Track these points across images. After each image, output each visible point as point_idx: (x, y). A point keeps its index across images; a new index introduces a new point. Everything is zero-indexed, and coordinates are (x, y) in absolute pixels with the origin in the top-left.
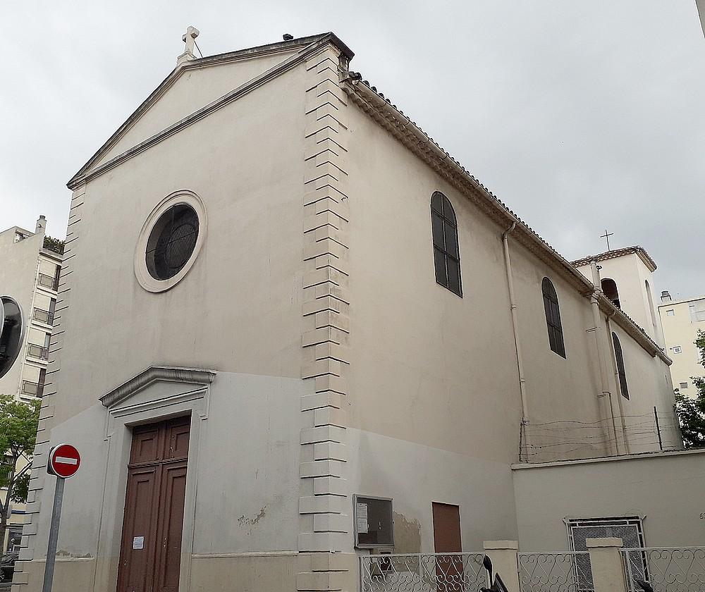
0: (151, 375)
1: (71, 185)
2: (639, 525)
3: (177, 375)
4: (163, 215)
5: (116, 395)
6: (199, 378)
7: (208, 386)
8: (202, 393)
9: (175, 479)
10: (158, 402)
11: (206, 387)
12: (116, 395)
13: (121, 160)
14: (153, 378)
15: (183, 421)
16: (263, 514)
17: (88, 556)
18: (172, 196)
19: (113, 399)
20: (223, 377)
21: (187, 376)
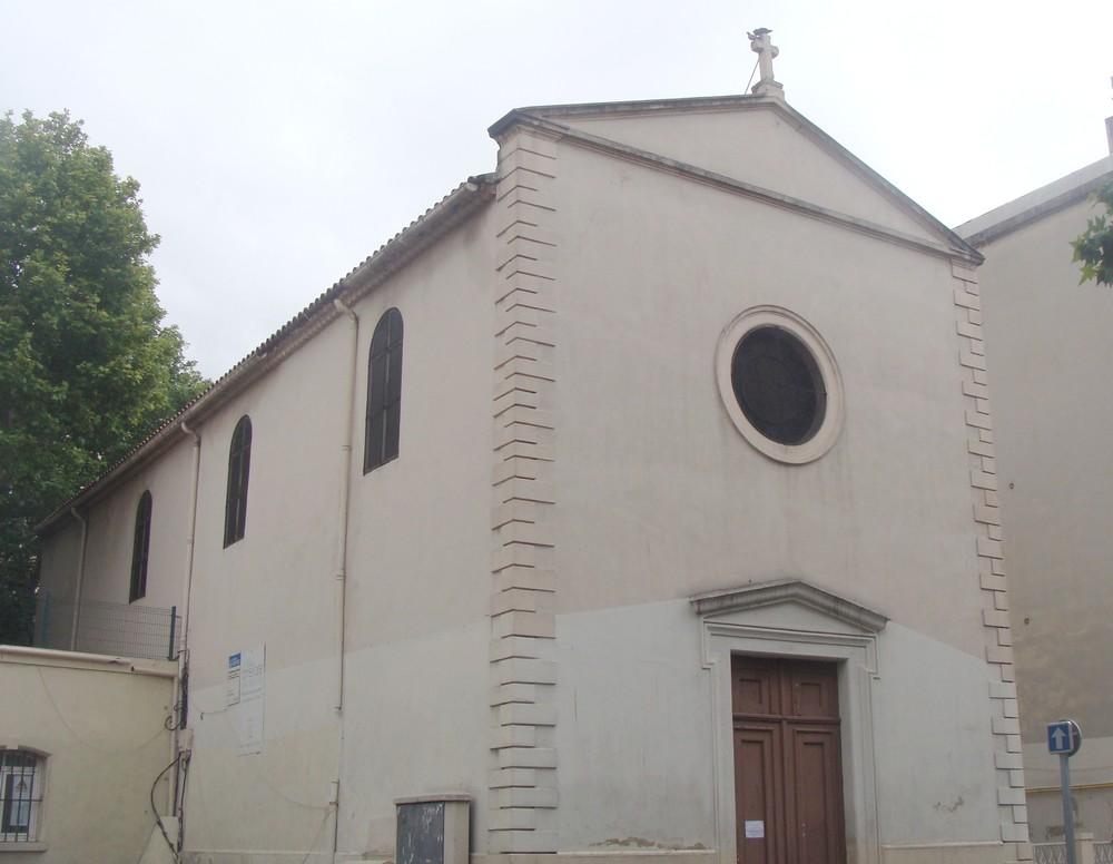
0: (791, 591)
3: (833, 606)
5: (728, 602)
6: (865, 622)
9: (466, 808)
10: (787, 633)
12: (728, 602)
14: (792, 596)
15: (826, 673)
16: (961, 802)
17: (699, 846)
19: (713, 607)
21: (852, 613)
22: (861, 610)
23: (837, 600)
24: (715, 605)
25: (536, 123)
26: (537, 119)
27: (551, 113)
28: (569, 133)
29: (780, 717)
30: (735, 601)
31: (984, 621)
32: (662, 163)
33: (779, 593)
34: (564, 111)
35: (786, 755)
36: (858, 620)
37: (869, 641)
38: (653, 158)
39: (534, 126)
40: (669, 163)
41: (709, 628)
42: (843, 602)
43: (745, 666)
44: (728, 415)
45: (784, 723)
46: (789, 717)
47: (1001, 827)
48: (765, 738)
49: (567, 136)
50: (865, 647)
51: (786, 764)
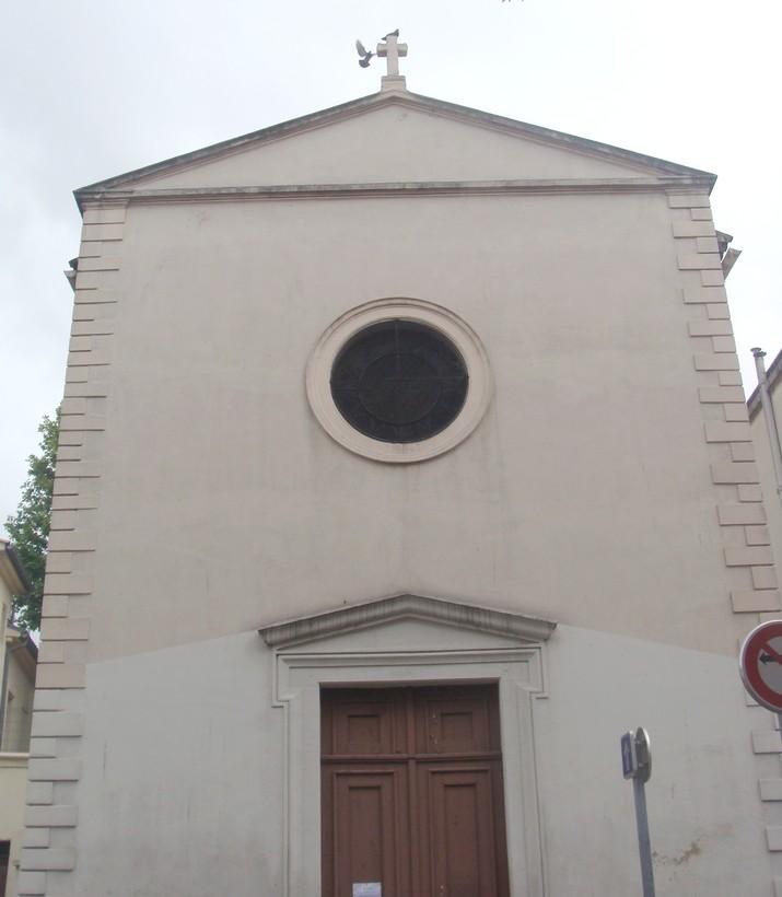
0: (398, 607)
1: (84, 198)
2: (289, 706)
3: (468, 618)
4: (397, 321)
6: (525, 633)
7: (542, 645)
8: (526, 654)
11: (537, 645)
12: (305, 629)
13: (239, 196)
14: (402, 612)
15: (486, 693)
16: (695, 850)
18: (380, 303)
19: (288, 637)
20: (558, 626)
22: (508, 617)
23: (467, 609)
24: (288, 634)
25: (98, 197)
26: (99, 193)
27: (115, 183)
28: (134, 195)
29: (405, 756)
30: (316, 627)
31: (689, 331)
32: (244, 194)
33: (379, 611)
34: (131, 178)
35: (474, 768)
36: (508, 630)
37: (532, 654)
38: (233, 191)
39: (97, 200)
40: (252, 191)
41: (286, 661)
42: (478, 611)
43: (333, 698)
44: (321, 427)
45: (412, 763)
46: (419, 756)
47: (766, 831)
48: (386, 783)
49: (135, 198)
50: (527, 661)
51: (463, 782)
